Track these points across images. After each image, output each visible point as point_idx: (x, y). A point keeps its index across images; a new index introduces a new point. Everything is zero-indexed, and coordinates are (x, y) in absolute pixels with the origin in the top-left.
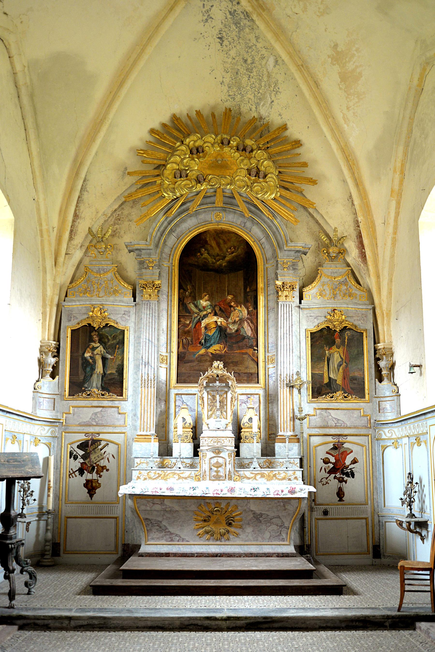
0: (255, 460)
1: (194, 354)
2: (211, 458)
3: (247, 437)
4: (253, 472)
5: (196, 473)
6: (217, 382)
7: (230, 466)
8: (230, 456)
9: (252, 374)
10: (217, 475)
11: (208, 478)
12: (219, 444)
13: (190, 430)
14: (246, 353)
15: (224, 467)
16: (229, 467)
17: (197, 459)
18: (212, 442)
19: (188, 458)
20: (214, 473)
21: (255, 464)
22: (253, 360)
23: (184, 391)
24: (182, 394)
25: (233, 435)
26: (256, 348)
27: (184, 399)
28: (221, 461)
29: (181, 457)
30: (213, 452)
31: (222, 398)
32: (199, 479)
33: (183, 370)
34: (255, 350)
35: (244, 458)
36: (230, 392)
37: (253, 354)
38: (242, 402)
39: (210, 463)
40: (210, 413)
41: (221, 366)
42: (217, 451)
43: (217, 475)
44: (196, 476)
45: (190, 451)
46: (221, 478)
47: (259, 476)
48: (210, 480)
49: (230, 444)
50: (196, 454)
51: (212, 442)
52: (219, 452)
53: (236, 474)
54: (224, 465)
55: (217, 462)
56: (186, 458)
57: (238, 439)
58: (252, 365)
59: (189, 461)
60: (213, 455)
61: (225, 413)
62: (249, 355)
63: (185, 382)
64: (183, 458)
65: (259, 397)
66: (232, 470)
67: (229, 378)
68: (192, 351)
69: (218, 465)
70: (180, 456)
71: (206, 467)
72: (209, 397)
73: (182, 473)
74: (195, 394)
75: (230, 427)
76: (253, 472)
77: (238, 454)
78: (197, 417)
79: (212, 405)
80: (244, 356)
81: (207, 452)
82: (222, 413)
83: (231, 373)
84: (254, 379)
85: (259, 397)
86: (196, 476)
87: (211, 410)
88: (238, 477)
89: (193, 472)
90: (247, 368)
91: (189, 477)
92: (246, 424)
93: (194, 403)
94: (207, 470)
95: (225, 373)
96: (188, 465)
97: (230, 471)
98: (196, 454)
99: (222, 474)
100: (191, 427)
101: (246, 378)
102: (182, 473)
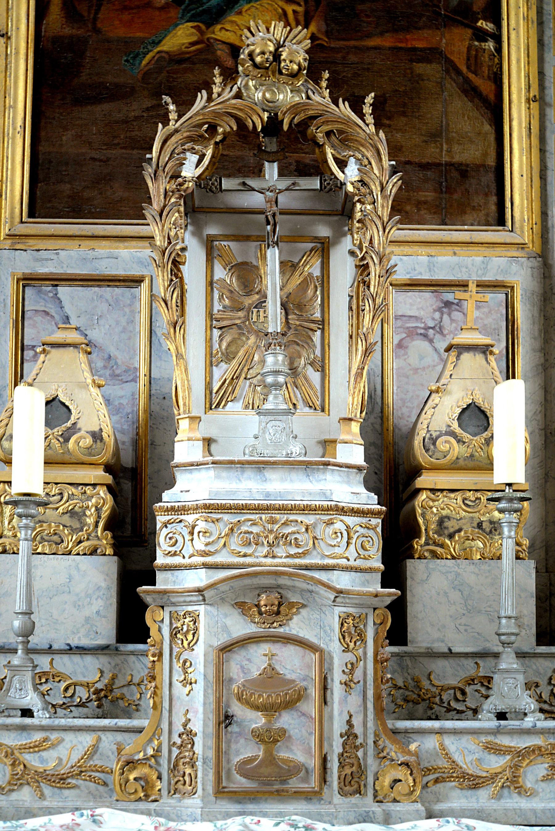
0: (508, 662)
1: (132, 49)
2: (227, 649)
3: (451, 525)
4: (505, 741)
5: (131, 744)
6: (271, 171)
7: (355, 700)
8: (351, 633)
9: (463, 171)
10: (270, 759)
11: (204, 776)
12: (280, 551)
13: (98, 474)
14: (433, 54)
15: (311, 707)
16: (346, 706)
17: (137, 661)
18: (235, 543)
19: (81, 650)
20: (246, 750)
21: (510, 688)
22: (471, 91)
23: (69, 258)
24: (56, 280)
25: (370, 500)
26: (488, 26)
27: (69, 309)
28: (292, 664)
29: (34, 640)
30: (241, 606)
31: (296, 281)
32: (146, 785)
33: (67, 142)
34: (481, 35)
35: (432, 655)
36: (347, 243)
37: (474, 60)
38: (411, 333)
39: (220, 680)
40: (220, 372)
41: (296, 54)
42: (268, 600)
43: (270, 759)
44: (131, 764)
45: (98, 605)
46: (294, 784)
47: (541, 768)
48: (221, 792)
49: (350, 556)
50: (132, 624)
51: (235, 543)
52: (281, 610)
53: (392, 750)
54: (314, 693)
55: (271, 676)
56: (71, 650)
57: (400, 540)
58: (463, 118)
59: (87, 671)
60: (240, 626)
61: (315, 377)
62: (451, 67)
63: (77, 210)
64: (50, 650)
65: (509, 306)
66: (366, 726)
67: (344, 138)
68: (121, 32)
69: (277, 697)
70: (27, 632)
71: (193, 704)
72: (220, 273)
73: (36, 748)
74: (137, 281)
75: (354, 453)
76: (505, 741)
77: (398, 633)
78: (150, 413)
79: (234, 323)
80: (421, 68)
81: (201, 609)
82: (294, 371)
83: (358, 111)
84: (478, 200)
85: (509, 306)
86: (131, 764)
87: (228, 357)
88: (401, 773)
89: (108, 742)
90: (435, 136)
91: (80, 771)
92: (442, 445)
93: (128, 330)
94: (200, 722)
95: (321, 98)
96: (83, 694)
97: (349, 735)
98: (132, 624)
99: (300, 751)
100: (106, 456)
101: (429, 195)
102: (36, 748)
